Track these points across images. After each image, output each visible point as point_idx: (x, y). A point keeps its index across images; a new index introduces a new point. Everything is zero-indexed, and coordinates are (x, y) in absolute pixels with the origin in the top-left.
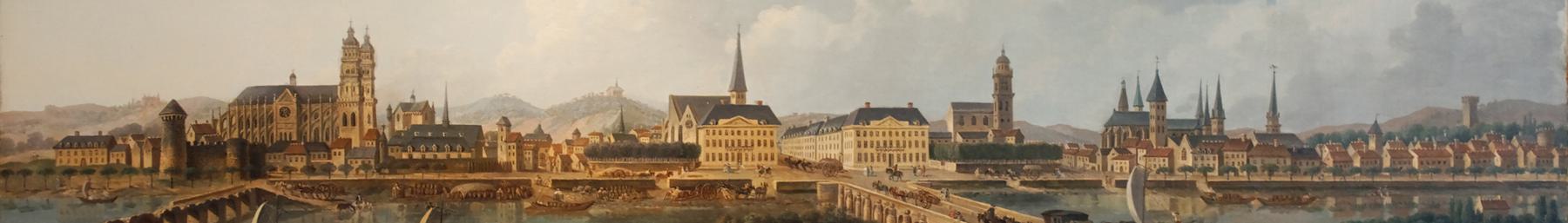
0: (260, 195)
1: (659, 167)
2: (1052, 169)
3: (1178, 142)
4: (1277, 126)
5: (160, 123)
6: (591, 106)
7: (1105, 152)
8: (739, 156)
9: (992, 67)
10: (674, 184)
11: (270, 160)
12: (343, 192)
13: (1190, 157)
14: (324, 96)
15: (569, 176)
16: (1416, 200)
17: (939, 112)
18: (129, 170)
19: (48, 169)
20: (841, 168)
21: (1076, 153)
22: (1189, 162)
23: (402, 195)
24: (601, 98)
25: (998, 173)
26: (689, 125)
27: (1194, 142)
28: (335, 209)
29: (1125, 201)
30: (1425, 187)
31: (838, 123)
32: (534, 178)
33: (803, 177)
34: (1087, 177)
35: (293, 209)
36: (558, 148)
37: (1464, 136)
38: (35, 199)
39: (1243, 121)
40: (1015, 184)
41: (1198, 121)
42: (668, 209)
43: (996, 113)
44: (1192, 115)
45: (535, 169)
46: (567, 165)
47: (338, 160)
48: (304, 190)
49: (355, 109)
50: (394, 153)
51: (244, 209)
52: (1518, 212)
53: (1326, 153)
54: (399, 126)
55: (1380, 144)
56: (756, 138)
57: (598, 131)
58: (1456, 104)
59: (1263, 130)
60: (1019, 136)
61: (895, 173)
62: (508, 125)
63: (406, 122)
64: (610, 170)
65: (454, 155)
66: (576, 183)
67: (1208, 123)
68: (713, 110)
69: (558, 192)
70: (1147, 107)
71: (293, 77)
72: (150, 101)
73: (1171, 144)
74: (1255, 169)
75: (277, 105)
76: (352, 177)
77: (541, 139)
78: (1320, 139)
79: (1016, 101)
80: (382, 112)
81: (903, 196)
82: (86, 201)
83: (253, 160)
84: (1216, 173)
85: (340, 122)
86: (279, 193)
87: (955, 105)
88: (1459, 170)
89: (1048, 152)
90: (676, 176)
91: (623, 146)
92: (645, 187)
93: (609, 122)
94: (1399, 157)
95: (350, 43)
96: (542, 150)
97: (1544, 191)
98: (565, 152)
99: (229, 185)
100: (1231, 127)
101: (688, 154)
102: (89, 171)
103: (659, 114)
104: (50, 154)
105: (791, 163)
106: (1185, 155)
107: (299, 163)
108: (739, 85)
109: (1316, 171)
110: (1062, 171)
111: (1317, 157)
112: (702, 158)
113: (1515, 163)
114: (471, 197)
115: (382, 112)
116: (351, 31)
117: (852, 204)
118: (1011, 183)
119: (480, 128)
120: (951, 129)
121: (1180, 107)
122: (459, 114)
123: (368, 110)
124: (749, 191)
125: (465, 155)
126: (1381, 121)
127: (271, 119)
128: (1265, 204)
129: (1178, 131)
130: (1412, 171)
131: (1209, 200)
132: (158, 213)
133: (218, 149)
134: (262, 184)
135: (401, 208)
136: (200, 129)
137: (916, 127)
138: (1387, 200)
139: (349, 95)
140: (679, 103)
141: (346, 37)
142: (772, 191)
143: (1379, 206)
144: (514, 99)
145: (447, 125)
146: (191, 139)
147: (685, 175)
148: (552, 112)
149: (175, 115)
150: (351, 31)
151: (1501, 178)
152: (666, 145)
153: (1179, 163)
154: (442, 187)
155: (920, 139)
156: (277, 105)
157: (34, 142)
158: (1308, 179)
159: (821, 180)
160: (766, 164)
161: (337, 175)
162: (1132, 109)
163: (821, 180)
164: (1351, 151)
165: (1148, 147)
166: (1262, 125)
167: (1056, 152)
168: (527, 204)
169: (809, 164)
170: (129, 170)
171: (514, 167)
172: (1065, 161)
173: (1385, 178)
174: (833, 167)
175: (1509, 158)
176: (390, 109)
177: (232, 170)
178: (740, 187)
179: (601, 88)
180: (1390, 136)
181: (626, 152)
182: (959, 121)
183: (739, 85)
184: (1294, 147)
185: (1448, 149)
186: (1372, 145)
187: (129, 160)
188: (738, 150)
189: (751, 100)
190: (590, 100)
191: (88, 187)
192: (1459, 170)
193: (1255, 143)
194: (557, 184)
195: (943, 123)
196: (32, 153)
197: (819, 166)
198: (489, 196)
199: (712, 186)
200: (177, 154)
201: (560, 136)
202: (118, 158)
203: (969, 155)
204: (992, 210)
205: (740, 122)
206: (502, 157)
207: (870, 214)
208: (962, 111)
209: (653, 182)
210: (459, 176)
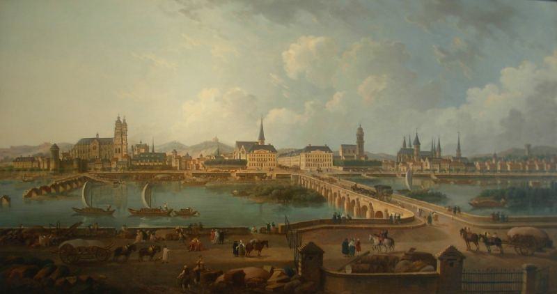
0: (85, 178)
1: (232, 168)
2: (378, 170)
3: (424, 160)
4: (460, 155)
5: (50, 152)
6: (207, 145)
7: (398, 164)
8: (262, 164)
9: (355, 131)
10: (238, 175)
11: (89, 165)
12: (115, 178)
13: (428, 165)
14: (108, 141)
15: (199, 172)
16: (509, 182)
17: (336, 147)
18: (39, 170)
19: (11, 169)
20: (300, 169)
21: (387, 164)
22: (428, 168)
23: (137, 179)
24: (210, 142)
25: (358, 171)
26: (243, 152)
27: (430, 160)
28: (112, 183)
29: (405, 182)
30: (512, 177)
31: (299, 152)
32: (185, 172)
33: (285, 173)
34: (392, 173)
35: (96, 184)
36: (194, 160)
37: (526, 159)
38: (7, 180)
39: (448, 152)
40: (364, 175)
41: (431, 152)
42: (235, 184)
43: (357, 148)
44: (429, 150)
45: (186, 169)
46: (198, 167)
47: (114, 165)
48: (101, 177)
49: (120, 147)
50: (133, 163)
51: (80, 184)
52: (544, 187)
53: (477, 164)
54: (136, 153)
55: (497, 161)
56: (268, 158)
57: (209, 154)
58: (522, 147)
59: (455, 156)
60: (366, 158)
61: (320, 171)
62: (176, 152)
63: (138, 152)
64: (214, 169)
65: (156, 164)
66: (201, 174)
67: (435, 153)
68: (251, 147)
69: (194, 178)
70: (413, 147)
71: (98, 135)
72: (47, 144)
73: (422, 161)
74: (452, 170)
75: (92, 146)
76: (119, 171)
77: (188, 158)
78: (475, 159)
79: (365, 145)
80: (129, 147)
81: (323, 179)
82: (24, 181)
83: (83, 166)
84: (438, 171)
85: (114, 151)
86: (92, 178)
87: (342, 145)
88: (524, 171)
89: (376, 163)
90: (238, 172)
91: (218, 160)
92: (227, 175)
93: (214, 151)
94: (504, 166)
95: (118, 122)
96: (188, 162)
97: (553, 179)
98: (197, 163)
99: (74, 175)
100: (443, 154)
101: (243, 163)
102: (25, 170)
103: (231, 149)
104: (11, 164)
105: (281, 167)
106: (427, 165)
107: (99, 167)
108: (262, 138)
109: (473, 171)
110: (383, 170)
111: (474, 166)
112: (248, 165)
113: (543, 169)
114: (162, 179)
115: (129, 147)
116: (119, 118)
117: (304, 182)
118: (362, 175)
119: (165, 154)
120: (341, 155)
121: (425, 146)
122: (158, 149)
123: (125, 147)
124: (265, 178)
125: (160, 164)
126: (497, 153)
127: (89, 150)
128: (455, 183)
129: (424, 156)
130: (508, 171)
131: (436, 182)
132: (49, 185)
133: (70, 162)
134: (86, 175)
135: (136, 184)
136: (64, 154)
137: (328, 153)
138: (499, 182)
139: (117, 142)
140: (239, 144)
141: (117, 119)
142: (274, 177)
143: (496, 184)
144: (179, 143)
145: (153, 152)
146: (61, 158)
147: (240, 171)
148: (192, 147)
149: (55, 149)
150: (119, 118)
151: (538, 174)
152: (234, 160)
153: (425, 168)
154: (151, 175)
155: (329, 158)
156: (92, 146)
157: (6, 159)
158: (471, 174)
159: (292, 173)
160: (272, 168)
161: (113, 171)
162: (407, 147)
163: (292, 173)
164: (486, 164)
165: (414, 162)
166: (454, 154)
167: (380, 163)
168: (182, 182)
169: (288, 167)
170: (39, 170)
171: (178, 168)
172: (383, 167)
173: (499, 174)
174: (297, 169)
175: (541, 166)
176: (132, 147)
177: (75, 169)
178: (262, 176)
179: (210, 139)
180: (500, 159)
181: (220, 163)
182: (344, 151)
183: (262, 138)
184: (466, 162)
185: (520, 164)
186: (494, 162)
187: (39, 166)
188: (262, 162)
189: (266, 143)
190: (206, 143)
191: (25, 176)
192: (524, 171)
193: (452, 160)
194: (194, 174)
195: (338, 152)
196: (5, 163)
197: (291, 168)
198: (168, 179)
199: (252, 176)
200: (56, 163)
201: (195, 156)
202: (35, 165)
203: (348, 164)
204: (356, 185)
205: (262, 151)
206: (174, 165)
207: (311, 186)
208: (345, 148)
209: (229, 174)
210: (158, 172)
